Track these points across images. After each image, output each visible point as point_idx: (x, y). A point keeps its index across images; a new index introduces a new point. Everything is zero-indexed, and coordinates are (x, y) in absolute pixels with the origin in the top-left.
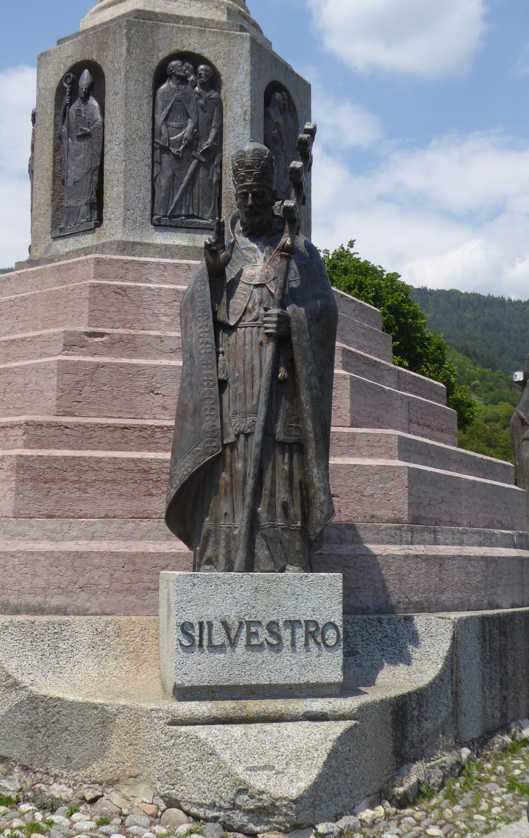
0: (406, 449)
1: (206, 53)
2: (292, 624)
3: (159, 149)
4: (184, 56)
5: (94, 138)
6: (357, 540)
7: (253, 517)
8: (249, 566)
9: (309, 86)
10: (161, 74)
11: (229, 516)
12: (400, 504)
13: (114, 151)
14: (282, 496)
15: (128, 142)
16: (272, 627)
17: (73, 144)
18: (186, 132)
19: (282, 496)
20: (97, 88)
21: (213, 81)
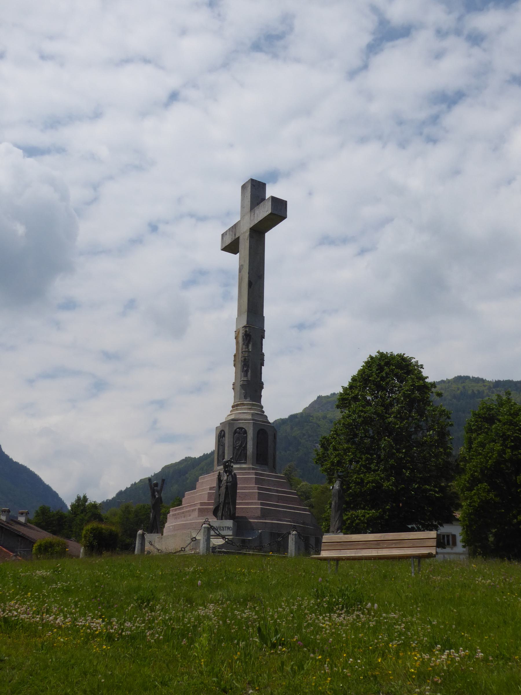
0: (262, 504)
1: (244, 427)
2: (225, 527)
3: (234, 448)
4: (239, 428)
5: (223, 446)
6: (247, 519)
7: (222, 513)
8: (222, 519)
9: (382, 356)
10: (235, 432)
11: (220, 514)
12: (259, 513)
13: (226, 448)
14: (226, 510)
15: (228, 447)
16: (223, 527)
17: (221, 447)
18: (239, 444)
19: (226, 510)
20: (224, 436)
21: (245, 432)
